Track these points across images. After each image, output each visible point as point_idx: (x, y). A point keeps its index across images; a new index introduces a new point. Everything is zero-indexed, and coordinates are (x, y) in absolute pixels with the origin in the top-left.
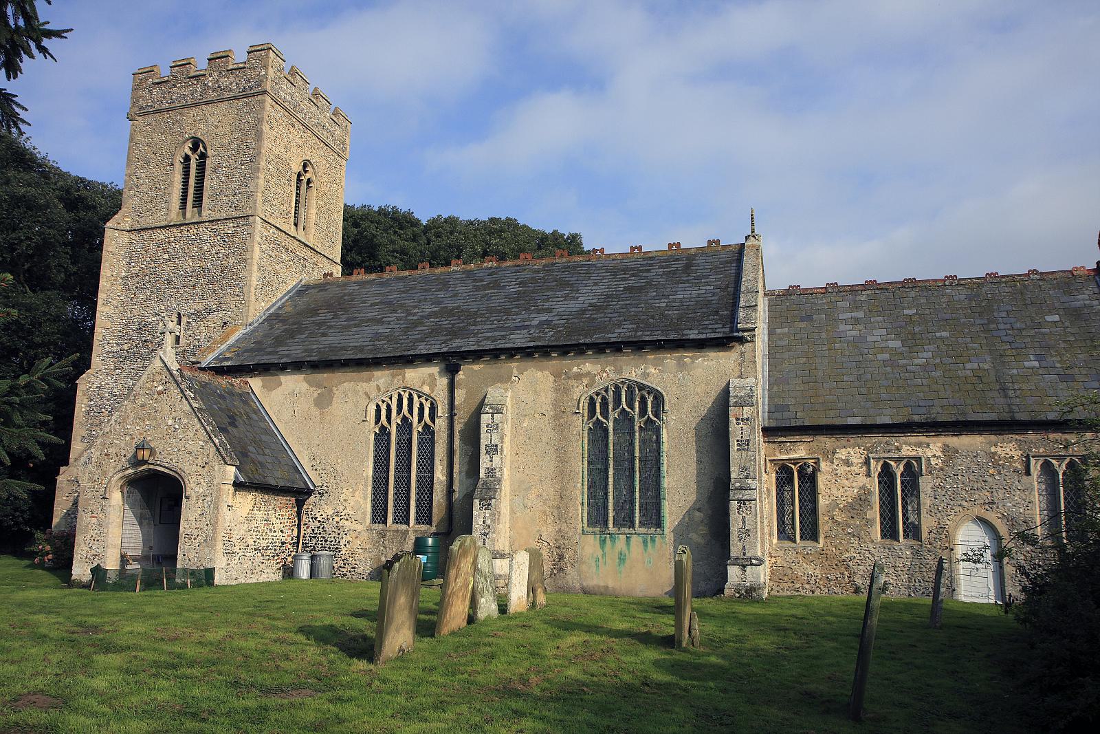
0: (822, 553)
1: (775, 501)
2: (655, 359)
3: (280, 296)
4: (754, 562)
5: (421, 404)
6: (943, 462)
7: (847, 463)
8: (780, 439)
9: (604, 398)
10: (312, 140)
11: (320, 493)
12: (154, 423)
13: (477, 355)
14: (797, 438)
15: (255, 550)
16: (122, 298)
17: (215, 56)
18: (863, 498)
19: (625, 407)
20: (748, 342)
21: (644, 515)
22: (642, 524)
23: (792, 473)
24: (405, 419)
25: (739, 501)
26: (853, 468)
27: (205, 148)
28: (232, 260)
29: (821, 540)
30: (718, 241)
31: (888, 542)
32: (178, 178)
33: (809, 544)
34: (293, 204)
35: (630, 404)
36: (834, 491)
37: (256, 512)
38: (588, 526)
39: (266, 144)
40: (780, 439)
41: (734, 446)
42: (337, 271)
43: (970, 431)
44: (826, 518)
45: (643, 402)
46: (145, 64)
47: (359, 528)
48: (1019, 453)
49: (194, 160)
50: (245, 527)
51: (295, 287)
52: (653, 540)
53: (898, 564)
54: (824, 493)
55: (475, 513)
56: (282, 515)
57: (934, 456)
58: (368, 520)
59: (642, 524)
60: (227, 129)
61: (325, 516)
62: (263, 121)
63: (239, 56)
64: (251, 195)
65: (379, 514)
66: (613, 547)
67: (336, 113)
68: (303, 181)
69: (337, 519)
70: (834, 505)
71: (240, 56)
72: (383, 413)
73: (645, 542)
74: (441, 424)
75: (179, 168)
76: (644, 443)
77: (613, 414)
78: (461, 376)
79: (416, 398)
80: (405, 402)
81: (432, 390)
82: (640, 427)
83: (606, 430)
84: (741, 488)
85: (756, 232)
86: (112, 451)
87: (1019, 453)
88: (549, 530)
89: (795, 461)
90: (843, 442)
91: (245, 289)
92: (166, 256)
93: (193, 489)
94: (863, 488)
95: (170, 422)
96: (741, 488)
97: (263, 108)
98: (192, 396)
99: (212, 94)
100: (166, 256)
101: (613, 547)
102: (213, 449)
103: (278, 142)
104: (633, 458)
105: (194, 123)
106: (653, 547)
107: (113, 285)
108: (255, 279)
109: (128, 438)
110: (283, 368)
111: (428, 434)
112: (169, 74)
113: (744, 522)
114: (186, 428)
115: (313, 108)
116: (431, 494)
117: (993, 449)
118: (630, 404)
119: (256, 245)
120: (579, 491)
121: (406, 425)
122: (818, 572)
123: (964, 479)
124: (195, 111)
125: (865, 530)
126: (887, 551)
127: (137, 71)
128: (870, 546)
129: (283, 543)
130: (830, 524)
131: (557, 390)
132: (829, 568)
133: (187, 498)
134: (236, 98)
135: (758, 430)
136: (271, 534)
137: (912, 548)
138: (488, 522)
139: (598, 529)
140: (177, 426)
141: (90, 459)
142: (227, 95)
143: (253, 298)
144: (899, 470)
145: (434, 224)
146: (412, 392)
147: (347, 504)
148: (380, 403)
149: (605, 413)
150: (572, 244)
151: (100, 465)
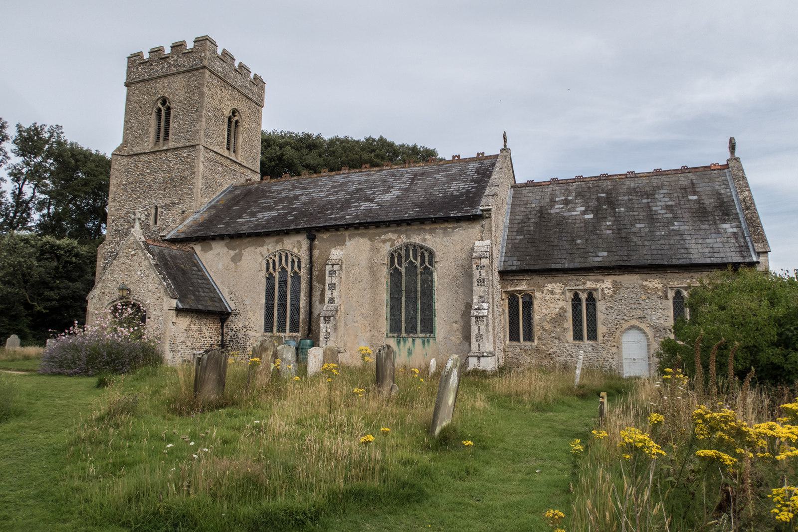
0: (537, 350)
1: (507, 316)
2: (430, 229)
4: (485, 354)
5: (293, 260)
6: (613, 291)
7: (552, 293)
8: (510, 278)
9: (399, 254)
10: (238, 96)
13: (327, 229)
14: (521, 277)
15: (192, 349)
17: (175, 45)
18: (562, 314)
19: (412, 259)
20: (487, 218)
21: (423, 326)
25: (477, 317)
28: (187, 173)
29: (536, 341)
30: (459, 155)
31: (577, 342)
32: (153, 122)
33: (528, 343)
34: (226, 137)
35: (415, 259)
37: (192, 326)
39: (207, 99)
40: (510, 278)
41: (475, 283)
42: (257, 178)
44: (539, 327)
45: (423, 256)
47: (257, 335)
48: (661, 285)
49: (163, 109)
50: (185, 335)
51: (228, 188)
52: (428, 341)
55: (321, 325)
56: (211, 328)
57: (606, 288)
59: (422, 332)
60: (183, 91)
61: (238, 328)
64: (197, 132)
66: (404, 346)
69: (245, 330)
70: (544, 318)
71: (190, 45)
72: (271, 265)
73: (424, 343)
74: (303, 273)
75: (154, 115)
76: (423, 282)
77: (404, 264)
78: (316, 242)
79: (289, 255)
80: (284, 258)
81: (299, 251)
82: (421, 272)
83: (401, 274)
84: (478, 309)
86: (106, 290)
87: (661, 285)
88: (368, 335)
89: (520, 292)
90: (550, 279)
91: (194, 190)
92: (148, 171)
94: (562, 308)
95: (139, 273)
96: (478, 309)
97: (204, 77)
98: (151, 256)
99: (173, 70)
100: (148, 171)
101: (404, 346)
104: (417, 291)
105: (162, 88)
106: (428, 345)
107: (117, 189)
108: (199, 183)
109: (115, 283)
110: (214, 238)
111: (296, 277)
113: (479, 329)
114: (147, 276)
115: (238, 76)
117: (644, 283)
118: (415, 258)
119: (201, 163)
120: (385, 311)
121: (283, 271)
122: (533, 361)
123: (625, 302)
124: (165, 80)
125: (563, 335)
126: (577, 347)
128: (566, 345)
129: (211, 345)
131: (371, 250)
132: (540, 358)
134: (187, 71)
135: (496, 273)
136: (203, 340)
137: (592, 345)
139: (396, 335)
140: (142, 275)
142: (182, 69)
144: (583, 296)
145: (332, 142)
146: (287, 252)
147: (250, 321)
148: (269, 259)
149: (400, 264)
150: (428, 156)
151: (100, 299)
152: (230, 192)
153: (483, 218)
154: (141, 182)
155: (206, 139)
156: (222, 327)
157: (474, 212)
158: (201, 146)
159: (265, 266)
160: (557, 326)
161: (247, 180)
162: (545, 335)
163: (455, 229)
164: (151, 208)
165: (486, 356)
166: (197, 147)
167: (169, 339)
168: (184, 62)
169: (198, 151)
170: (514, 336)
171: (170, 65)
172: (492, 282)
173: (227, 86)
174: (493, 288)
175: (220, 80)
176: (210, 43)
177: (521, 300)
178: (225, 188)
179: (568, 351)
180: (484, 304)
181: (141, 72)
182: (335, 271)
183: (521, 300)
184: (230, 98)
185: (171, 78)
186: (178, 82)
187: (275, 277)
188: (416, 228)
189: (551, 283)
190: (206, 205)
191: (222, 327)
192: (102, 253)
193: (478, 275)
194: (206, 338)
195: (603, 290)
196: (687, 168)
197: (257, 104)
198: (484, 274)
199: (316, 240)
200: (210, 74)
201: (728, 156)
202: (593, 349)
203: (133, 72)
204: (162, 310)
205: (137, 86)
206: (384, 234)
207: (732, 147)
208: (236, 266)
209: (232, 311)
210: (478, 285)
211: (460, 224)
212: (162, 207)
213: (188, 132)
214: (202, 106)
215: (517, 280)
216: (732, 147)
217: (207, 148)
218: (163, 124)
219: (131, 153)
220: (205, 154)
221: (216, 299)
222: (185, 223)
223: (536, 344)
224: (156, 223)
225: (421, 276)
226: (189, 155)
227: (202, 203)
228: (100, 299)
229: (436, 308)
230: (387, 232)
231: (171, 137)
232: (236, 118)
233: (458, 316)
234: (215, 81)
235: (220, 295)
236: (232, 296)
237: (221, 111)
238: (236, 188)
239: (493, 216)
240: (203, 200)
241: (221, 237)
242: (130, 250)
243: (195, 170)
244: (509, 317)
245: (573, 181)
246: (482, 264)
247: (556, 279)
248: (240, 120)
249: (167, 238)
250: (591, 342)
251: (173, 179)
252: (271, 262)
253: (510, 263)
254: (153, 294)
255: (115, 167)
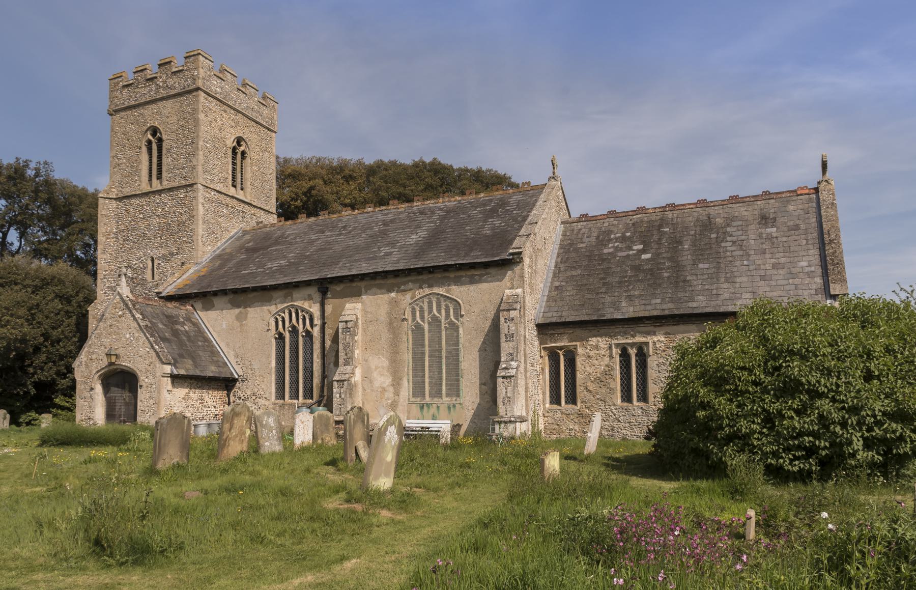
3: (224, 241)
5: (304, 317)
7: (597, 347)
11: (242, 381)
12: (118, 337)
14: (562, 331)
16: (115, 248)
18: (607, 373)
22: (447, 395)
23: (559, 356)
24: (294, 327)
25: (503, 377)
26: (601, 352)
27: (161, 133)
29: (579, 404)
30: (529, 182)
31: (626, 404)
32: (145, 157)
33: (570, 406)
35: (439, 311)
36: (588, 369)
37: (191, 394)
38: (413, 397)
39: (202, 128)
41: (503, 339)
43: (686, 321)
45: (304, 320)
46: (117, 71)
51: (237, 233)
53: (632, 421)
54: (581, 370)
55: (335, 390)
56: (215, 396)
58: (273, 398)
59: (447, 395)
60: (175, 118)
61: (246, 396)
62: (198, 111)
63: (178, 63)
64: (194, 168)
65: (280, 394)
66: (428, 411)
67: (264, 97)
68: (238, 152)
69: (254, 397)
74: (316, 332)
75: (144, 149)
82: (445, 327)
85: (556, 174)
86: (94, 356)
89: (561, 348)
91: (194, 238)
92: (141, 216)
93: (143, 380)
96: (506, 368)
97: (198, 101)
99: (163, 93)
100: (141, 216)
102: (154, 354)
103: (213, 125)
105: (151, 116)
107: (107, 238)
108: (201, 230)
109: (103, 348)
110: (215, 294)
111: (309, 335)
112: (183, 63)
114: (137, 340)
115: (242, 96)
116: (312, 378)
118: (439, 311)
119: (200, 205)
121: (294, 331)
122: (576, 427)
124: (154, 106)
126: (624, 410)
127: (112, 77)
128: (613, 407)
129: (216, 415)
130: (585, 393)
132: (584, 424)
133: (141, 386)
136: (205, 409)
137: (642, 408)
138: (343, 396)
140: (132, 339)
141: (81, 362)
142: (173, 92)
143: (200, 243)
144: (633, 352)
145: (416, 165)
148: (278, 317)
152: (239, 238)
153: (514, 263)
154: (134, 229)
155: (205, 176)
156: (228, 396)
157: (505, 256)
158: (199, 185)
159: (274, 324)
160: (602, 386)
161: (258, 223)
162: (589, 396)
163: (483, 276)
164: (146, 259)
165: (513, 422)
166: (195, 186)
167: (164, 409)
168: (174, 83)
169: (197, 190)
170: (555, 399)
171: (158, 87)
172: (525, 337)
173: (228, 109)
174: (525, 344)
175: (218, 103)
176: (204, 59)
177: (562, 358)
178: (232, 234)
179: (615, 415)
180: (513, 363)
181: (125, 97)
182: (350, 328)
183: (562, 358)
184: (233, 124)
185: (160, 104)
186: (168, 107)
187: (284, 337)
188: (439, 276)
189: (596, 336)
190: (209, 255)
191: (228, 396)
192: (94, 314)
193: (506, 329)
194: (209, 407)
195: (654, 343)
196: (770, 193)
197: (268, 129)
198: (513, 328)
199: (329, 293)
200: (206, 96)
201: (819, 177)
202: (643, 413)
203: (117, 97)
204: (154, 376)
205: (122, 114)
206: (404, 285)
207: (824, 166)
208: (242, 325)
209: (239, 376)
210: (506, 341)
211: (488, 270)
212: (159, 259)
213: (183, 168)
214: (198, 136)
215: (558, 334)
216: (824, 166)
217: (207, 187)
218: (155, 160)
219: (120, 195)
220: (205, 194)
221: (221, 364)
222: (184, 277)
223: (579, 408)
224: (153, 278)
225: (446, 332)
226: (186, 196)
227: (204, 252)
228: (87, 366)
229: (462, 367)
230: (407, 282)
231: (164, 174)
232: (242, 148)
233: (486, 377)
234: (213, 104)
235: (225, 358)
236: (238, 360)
237: (223, 140)
238: (245, 232)
239: (527, 261)
240: (205, 249)
241: (224, 292)
242: (117, 310)
243: (194, 214)
244: (550, 377)
245: (635, 213)
246: (511, 316)
247: (602, 331)
248: (247, 151)
249: (163, 294)
250: (641, 404)
251: (170, 225)
252: (280, 319)
253: (550, 314)
254: (145, 360)
255: (103, 213)
